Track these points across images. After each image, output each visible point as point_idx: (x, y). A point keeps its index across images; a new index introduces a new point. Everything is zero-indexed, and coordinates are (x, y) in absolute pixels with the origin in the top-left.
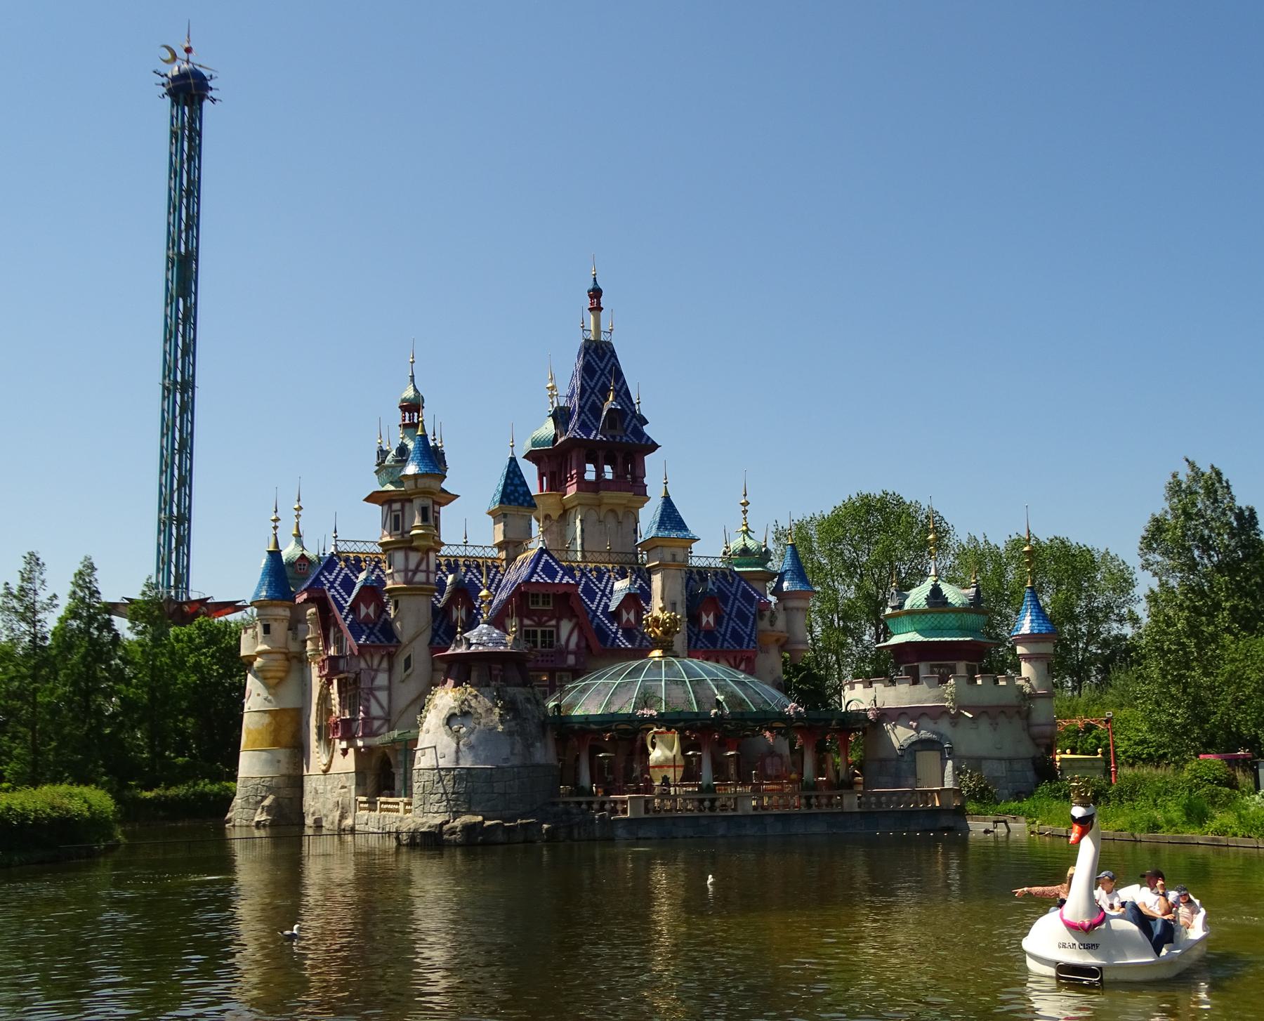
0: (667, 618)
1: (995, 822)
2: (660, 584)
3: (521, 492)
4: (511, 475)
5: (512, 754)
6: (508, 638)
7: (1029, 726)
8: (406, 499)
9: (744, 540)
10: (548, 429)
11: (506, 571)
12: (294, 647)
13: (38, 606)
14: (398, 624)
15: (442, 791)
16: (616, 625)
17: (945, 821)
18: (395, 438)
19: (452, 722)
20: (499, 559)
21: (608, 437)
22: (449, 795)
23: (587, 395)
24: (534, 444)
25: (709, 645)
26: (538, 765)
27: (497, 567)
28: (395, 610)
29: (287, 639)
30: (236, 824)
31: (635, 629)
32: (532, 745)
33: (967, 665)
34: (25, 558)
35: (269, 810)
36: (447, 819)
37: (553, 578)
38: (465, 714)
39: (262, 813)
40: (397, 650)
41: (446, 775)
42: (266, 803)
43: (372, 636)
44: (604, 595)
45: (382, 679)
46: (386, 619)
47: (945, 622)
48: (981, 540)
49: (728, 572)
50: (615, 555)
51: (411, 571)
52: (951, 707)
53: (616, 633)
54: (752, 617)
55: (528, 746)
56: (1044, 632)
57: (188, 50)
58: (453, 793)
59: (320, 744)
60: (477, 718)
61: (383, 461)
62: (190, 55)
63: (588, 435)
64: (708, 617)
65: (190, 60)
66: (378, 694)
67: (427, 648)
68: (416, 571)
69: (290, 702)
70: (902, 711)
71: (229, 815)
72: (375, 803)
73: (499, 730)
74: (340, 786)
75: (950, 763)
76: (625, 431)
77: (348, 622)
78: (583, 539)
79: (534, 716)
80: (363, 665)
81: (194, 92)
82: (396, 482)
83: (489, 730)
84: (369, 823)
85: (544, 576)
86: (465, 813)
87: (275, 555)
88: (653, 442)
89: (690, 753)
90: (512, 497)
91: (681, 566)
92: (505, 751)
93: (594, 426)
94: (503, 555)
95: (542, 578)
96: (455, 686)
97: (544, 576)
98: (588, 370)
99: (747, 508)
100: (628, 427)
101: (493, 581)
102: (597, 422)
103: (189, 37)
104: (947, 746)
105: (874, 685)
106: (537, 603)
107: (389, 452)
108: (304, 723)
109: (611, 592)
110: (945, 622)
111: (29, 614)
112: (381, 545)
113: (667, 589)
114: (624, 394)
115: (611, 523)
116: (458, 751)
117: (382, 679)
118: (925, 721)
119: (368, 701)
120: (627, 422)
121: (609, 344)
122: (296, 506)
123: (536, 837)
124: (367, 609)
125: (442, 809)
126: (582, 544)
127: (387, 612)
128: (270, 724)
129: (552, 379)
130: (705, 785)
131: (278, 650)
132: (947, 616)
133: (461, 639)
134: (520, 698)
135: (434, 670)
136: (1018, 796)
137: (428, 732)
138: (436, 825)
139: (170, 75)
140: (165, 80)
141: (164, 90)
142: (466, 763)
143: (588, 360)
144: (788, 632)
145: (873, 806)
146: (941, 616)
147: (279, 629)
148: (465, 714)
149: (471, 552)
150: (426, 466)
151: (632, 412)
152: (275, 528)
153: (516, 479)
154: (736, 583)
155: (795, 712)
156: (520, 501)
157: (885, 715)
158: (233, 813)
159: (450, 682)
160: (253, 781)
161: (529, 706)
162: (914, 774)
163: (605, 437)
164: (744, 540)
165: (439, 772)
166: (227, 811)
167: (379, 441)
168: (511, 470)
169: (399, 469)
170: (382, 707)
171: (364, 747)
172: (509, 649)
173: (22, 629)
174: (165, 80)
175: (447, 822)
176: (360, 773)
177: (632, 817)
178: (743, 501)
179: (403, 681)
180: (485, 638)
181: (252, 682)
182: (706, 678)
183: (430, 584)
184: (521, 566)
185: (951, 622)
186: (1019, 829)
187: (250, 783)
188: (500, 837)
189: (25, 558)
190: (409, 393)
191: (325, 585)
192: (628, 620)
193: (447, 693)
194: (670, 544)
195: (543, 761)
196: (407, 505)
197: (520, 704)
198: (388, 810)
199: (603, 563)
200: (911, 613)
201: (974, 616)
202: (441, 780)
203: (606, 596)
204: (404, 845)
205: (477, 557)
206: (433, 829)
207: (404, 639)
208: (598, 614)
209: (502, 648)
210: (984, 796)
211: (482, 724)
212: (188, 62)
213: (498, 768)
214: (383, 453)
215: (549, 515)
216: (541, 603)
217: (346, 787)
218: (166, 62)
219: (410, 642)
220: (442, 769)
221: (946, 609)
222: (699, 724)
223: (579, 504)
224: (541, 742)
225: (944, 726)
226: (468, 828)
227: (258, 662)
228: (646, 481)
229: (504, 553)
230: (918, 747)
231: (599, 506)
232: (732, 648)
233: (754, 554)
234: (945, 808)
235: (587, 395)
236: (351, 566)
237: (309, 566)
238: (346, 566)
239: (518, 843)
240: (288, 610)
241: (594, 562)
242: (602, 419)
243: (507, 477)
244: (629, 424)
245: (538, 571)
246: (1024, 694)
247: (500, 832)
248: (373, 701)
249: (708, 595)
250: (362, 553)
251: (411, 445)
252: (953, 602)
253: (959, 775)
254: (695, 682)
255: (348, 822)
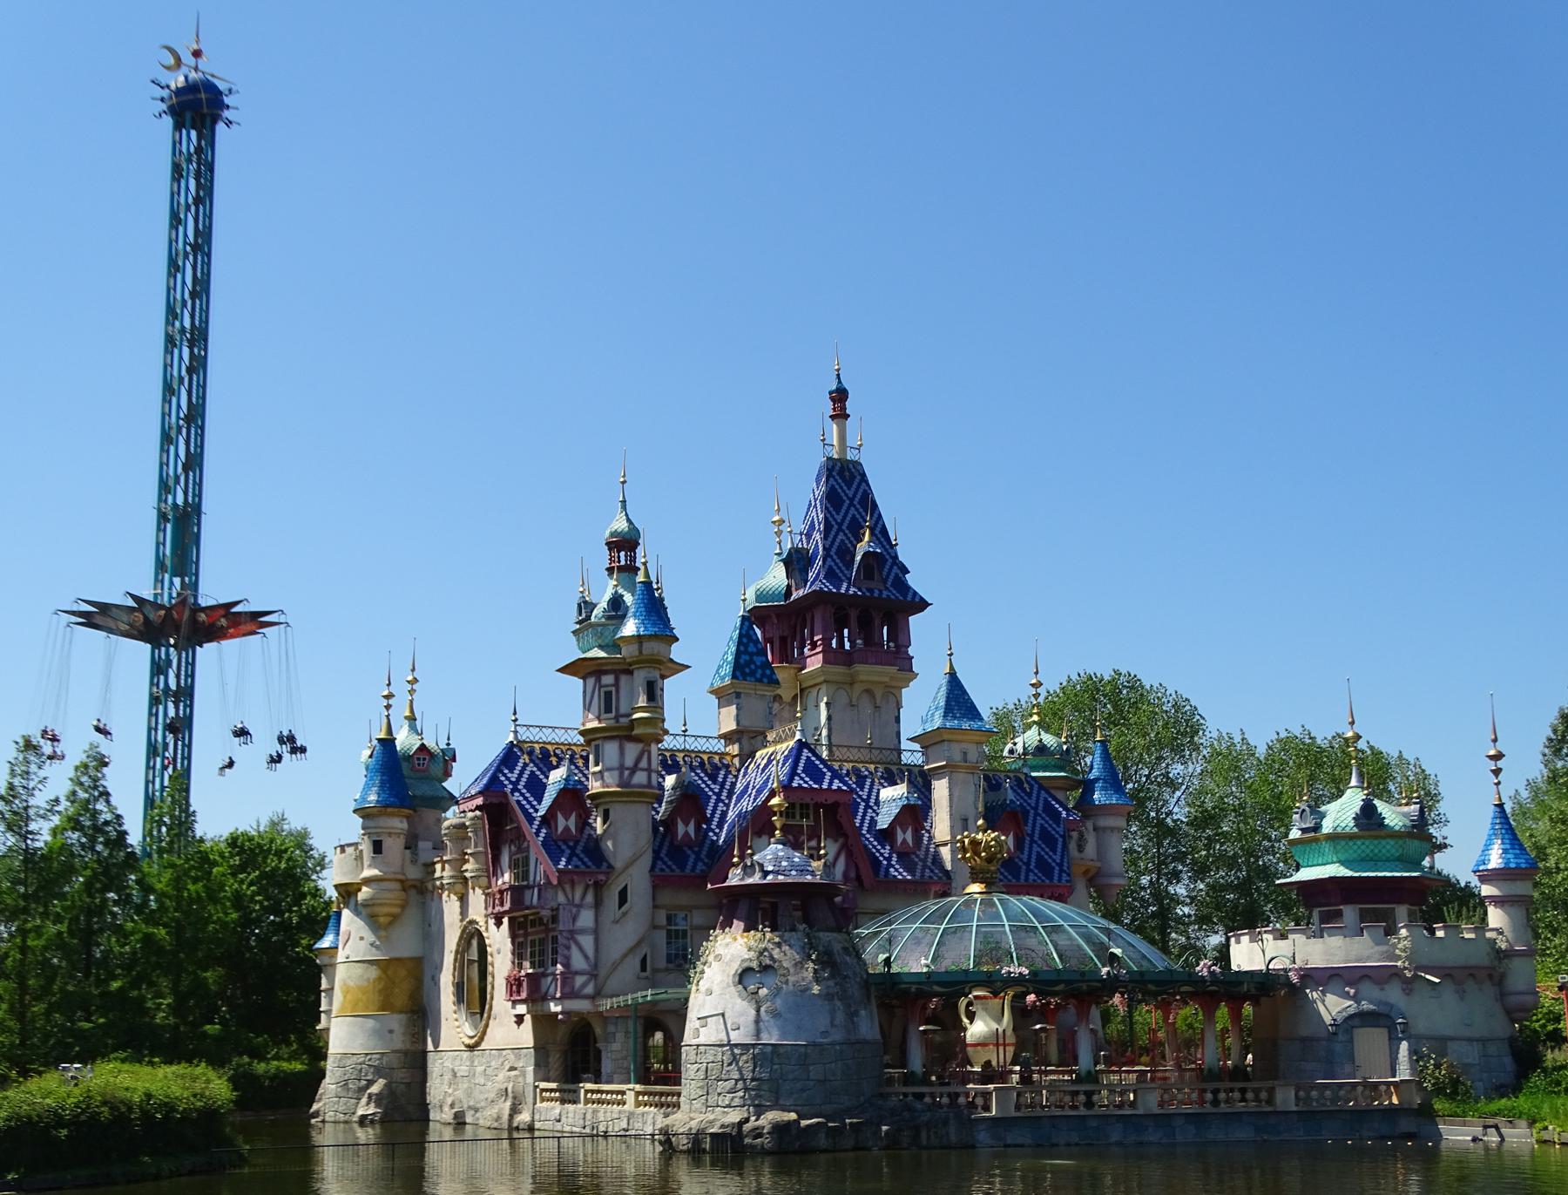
0: (992, 840)
1: (1486, 1127)
2: (946, 792)
3: (758, 663)
4: (745, 640)
5: (832, 1025)
6: (815, 864)
7: (1502, 995)
8: (624, 670)
9: (1039, 734)
10: (777, 577)
11: (739, 771)
12: (413, 873)
13: (31, 812)
14: (609, 844)
15: (736, 1077)
16: (888, 847)
17: (1406, 1125)
18: (604, 591)
19: (746, 980)
20: (727, 754)
21: (864, 590)
22: (748, 1082)
23: (833, 533)
24: (759, 597)
25: (1010, 877)
26: (865, 1042)
27: (727, 767)
28: (604, 823)
29: (403, 860)
30: (327, 1119)
31: (914, 853)
32: (856, 1013)
33: (1409, 910)
34: (17, 743)
35: (378, 1099)
36: (746, 1115)
37: (820, 782)
38: (765, 969)
39: (368, 1104)
40: (608, 879)
41: (741, 1054)
42: (375, 1089)
43: (575, 859)
44: (867, 807)
45: (586, 918)
46: (590, 835)
47: (1380, 851)
48: (1237, 739)
49: (1023, 777)
50: (846, 749)
51: (627, 769)
52: (1405, 968)
53: (889, 859)
54: (1060, 839)
55: (852, 1015)
56: (1523, 866)
57: (197, 54)
58: (753, 1080)
59: (459, 1009)
60: (784, 975)
61: (588, 617)
62: (200, 61)
63: (839, 588)
64: (904, 833)
65: (200, 67)
66: (581, 939)
67: (648, 876)
68: (634, 769)
69: (406, 944)
70: (1333, 972)
71: (315, 1107)
72: (576, 1091)
73: (816, 992)
74: (507, 1068)
75: (1404, 1046)
76: (885, 581)
77: (541, 839)
78: (830, 730)
79: (855, 973)
80: (561, 898)
81: (205, 110)
82: (607, 646)
83: (801, 991)
84: (563, 1119)
85: (807, 779)
86: (771, 1108)
87: (388, 743)
88: (922, 598)
89: (1038, 1026)
90: (747, 670)
91: (974, 768)
92: (823, 1022)
93: (845, 575)
94: (734, 749)
95: (806, 782)
96: (747, 930)
97: (807, 779)
98: (832, 499)
99: (414, 687)
100: (888, 576)
101: (722, 785)
102: (848, 569)
103: (197, 36)
104: (1400, 1020)
105: (1290, 936)
106: (794, 817)
107: (595, 605)
108: (427, 979)
109: (877, 802)
110: (1380, 851)
111: (18, 823)
112: (582, 733)
113: (955, 800)
114: (881, 533)
115: (867, 709)
116: (758, 1021)
117: (586, 918)
118: (1367, 988)
119: (568, 948)
120: (886, 570)
121: (857, 464)
122: (410, 678)
123: (871, 1143)
124: (567, 820)
125: (737, 1102)
126: (829, 736)
127: (590, 825)
128: (379, 979)
129: (779, 510)
130: (1083, 1073)
131: (393, 876)
132: (1384, 842)
133: (752, 865)
134: (837, 947)
135: (655, 907)
136: (1502, 1091)
137: (710, 993)
138: (733, 1124)
139: (173, 86)
140: (165, 93)
141: (164, 107)
142: (771, 1038)
143: (833, 486)
144: (1099, 860)
145: (1315, 1104)
146: (1376, 842)
147: (393, 846)
148: (765, 969)
149: (692, 744)
150: (654, 624)
151: (891, 557)
152: (388, 707)
153: (751, 645)
154: (1035, 792)
155: (1209, 972)
156: (758, 676)
157: (1312, 977)
158: (321, 1104)
159: (738, 925)
160: (355, 1058)
161: (848, 958)
162: (1352, 1058)
163: (860, 590)
164: (1039, 734)
165: (732, 1050)
166: (312, 1101)
167: (581, 589)
168: (744, 632)
169: (612, 628)
170: (586, 957)
171: (562, 1013)
172: (818, 880)
173: (9, 844)
174: (165, 93)
175: (747, 1120)
176: (541, 1049)
177: (999, 1116)
178: (1034, 681)
179: (616, 922)
180: (784, 864)
181: (352, 921)
182: (1037, 924)
183: (652, 787)
184: (766, 766)
185: (1388, 851)
186: (1519, 1137)
187: (349, 1062)
188: (822, 1141)
189: (17, 743)
190: (621, 525)
191: (506, 786)
192: (904, 841)
193: (735, 939)
194: (959, 737)
195: (869, 1037)
196: (624, 679)
197: (837, 956)
198: (599, 1102)
199: (862, 762)
200: (1334, 837)
201: (1416, 843)
202: (735, 1059)
203: (871, 807)
204: (681, 1151)
205: (699, 752)
206: (728, 1130)
207: (618, 864)
208: (864, 832)
209: (809, 877)
210: (1453, 1089)
211: (790, 984)
212: (196, 69)
213: (815, 1045)
214: (586, 606)
215: (780, 697)
216: (798, 817)
217: (515, 1069)
218: (168, 68)
219: (626, 868)
220: (736, 1045)
221: (1382, 833)
222: (1085, 987)
223: (825, 681)
224: (865, 1009)
225: (1394, 994)
226: (780, 1129)
227: (365, 893)
228: (911, 651)
229: (736, 747)
230: (1356, 1021)
231: (851, 684)
232: (935, 878)
233: (1052, 754)
234: (1406, 1106)
235: (833, 533)
236: (537, 761)
237: (430, 760)
238: (531, 761)
239: (846, 1150)
240: (405, 820)
241: (851, 761)
242: (856, 566)
243: (740, 643)
244: (889, 573)
245: (799, 772)
246: (1499, 951)
247: (822, 1136)
248: (574, 948)
249: (1008, 809)
250: (550, 743)
251: (628, 598)
252: (1392, 824)
253: (1417, 1061)
254: (1049, 929)
255: (524, 1117)
